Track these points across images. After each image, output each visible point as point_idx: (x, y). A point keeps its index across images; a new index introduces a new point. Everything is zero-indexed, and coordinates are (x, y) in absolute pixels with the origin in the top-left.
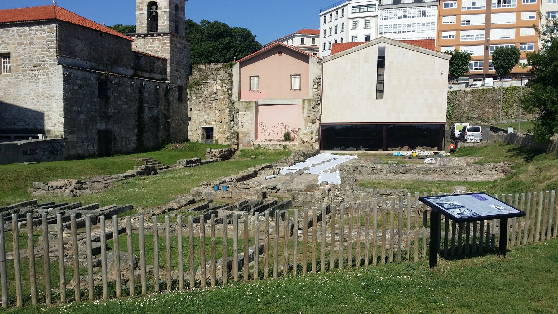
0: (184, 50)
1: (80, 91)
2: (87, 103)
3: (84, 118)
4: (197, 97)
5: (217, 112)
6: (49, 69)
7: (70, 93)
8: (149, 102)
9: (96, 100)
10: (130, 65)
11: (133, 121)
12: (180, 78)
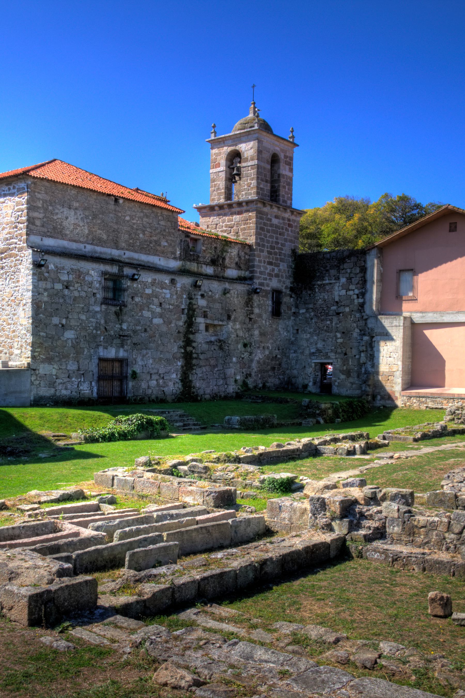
0: (287, 230)
1: (66, 292)
2: (79, 313)
3: (72, 336)
4: (307, 309)
5: (339, 335)
6: (17, 255)
7: (46, 294)
8: (209, 314)
9: (97, 309)
10: (174, 253)
11: (175, 347)
12: (277, 276)
